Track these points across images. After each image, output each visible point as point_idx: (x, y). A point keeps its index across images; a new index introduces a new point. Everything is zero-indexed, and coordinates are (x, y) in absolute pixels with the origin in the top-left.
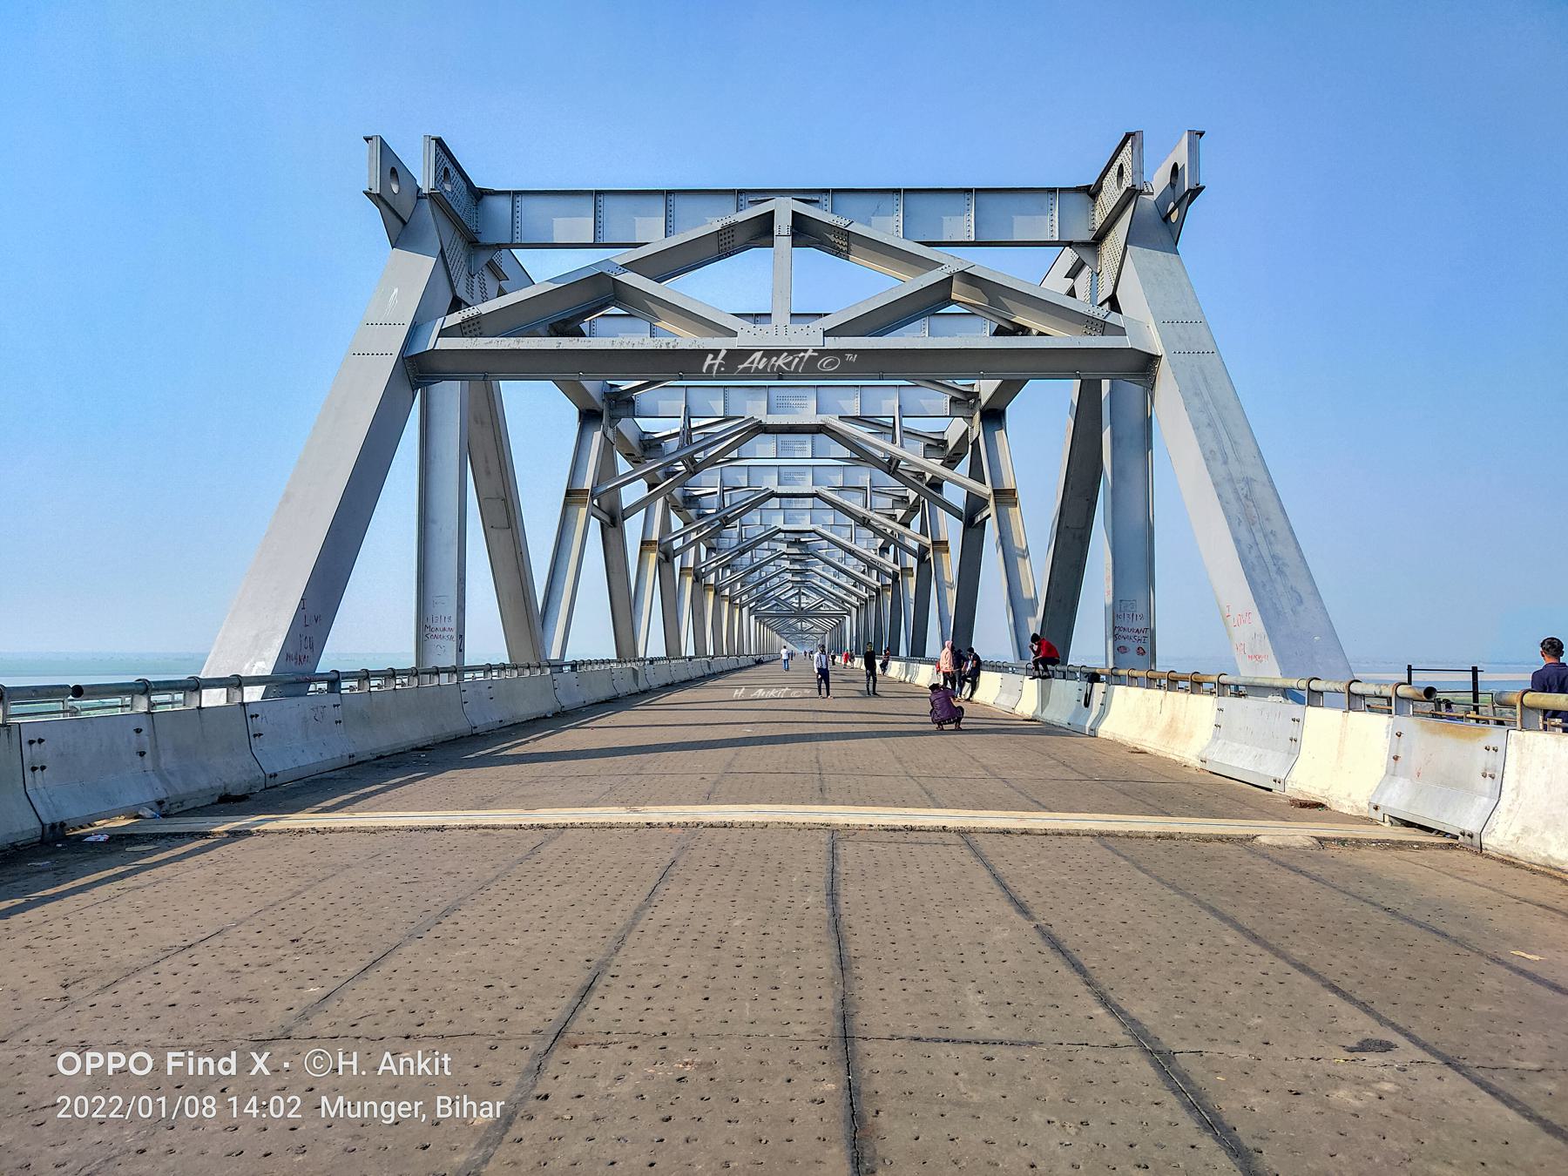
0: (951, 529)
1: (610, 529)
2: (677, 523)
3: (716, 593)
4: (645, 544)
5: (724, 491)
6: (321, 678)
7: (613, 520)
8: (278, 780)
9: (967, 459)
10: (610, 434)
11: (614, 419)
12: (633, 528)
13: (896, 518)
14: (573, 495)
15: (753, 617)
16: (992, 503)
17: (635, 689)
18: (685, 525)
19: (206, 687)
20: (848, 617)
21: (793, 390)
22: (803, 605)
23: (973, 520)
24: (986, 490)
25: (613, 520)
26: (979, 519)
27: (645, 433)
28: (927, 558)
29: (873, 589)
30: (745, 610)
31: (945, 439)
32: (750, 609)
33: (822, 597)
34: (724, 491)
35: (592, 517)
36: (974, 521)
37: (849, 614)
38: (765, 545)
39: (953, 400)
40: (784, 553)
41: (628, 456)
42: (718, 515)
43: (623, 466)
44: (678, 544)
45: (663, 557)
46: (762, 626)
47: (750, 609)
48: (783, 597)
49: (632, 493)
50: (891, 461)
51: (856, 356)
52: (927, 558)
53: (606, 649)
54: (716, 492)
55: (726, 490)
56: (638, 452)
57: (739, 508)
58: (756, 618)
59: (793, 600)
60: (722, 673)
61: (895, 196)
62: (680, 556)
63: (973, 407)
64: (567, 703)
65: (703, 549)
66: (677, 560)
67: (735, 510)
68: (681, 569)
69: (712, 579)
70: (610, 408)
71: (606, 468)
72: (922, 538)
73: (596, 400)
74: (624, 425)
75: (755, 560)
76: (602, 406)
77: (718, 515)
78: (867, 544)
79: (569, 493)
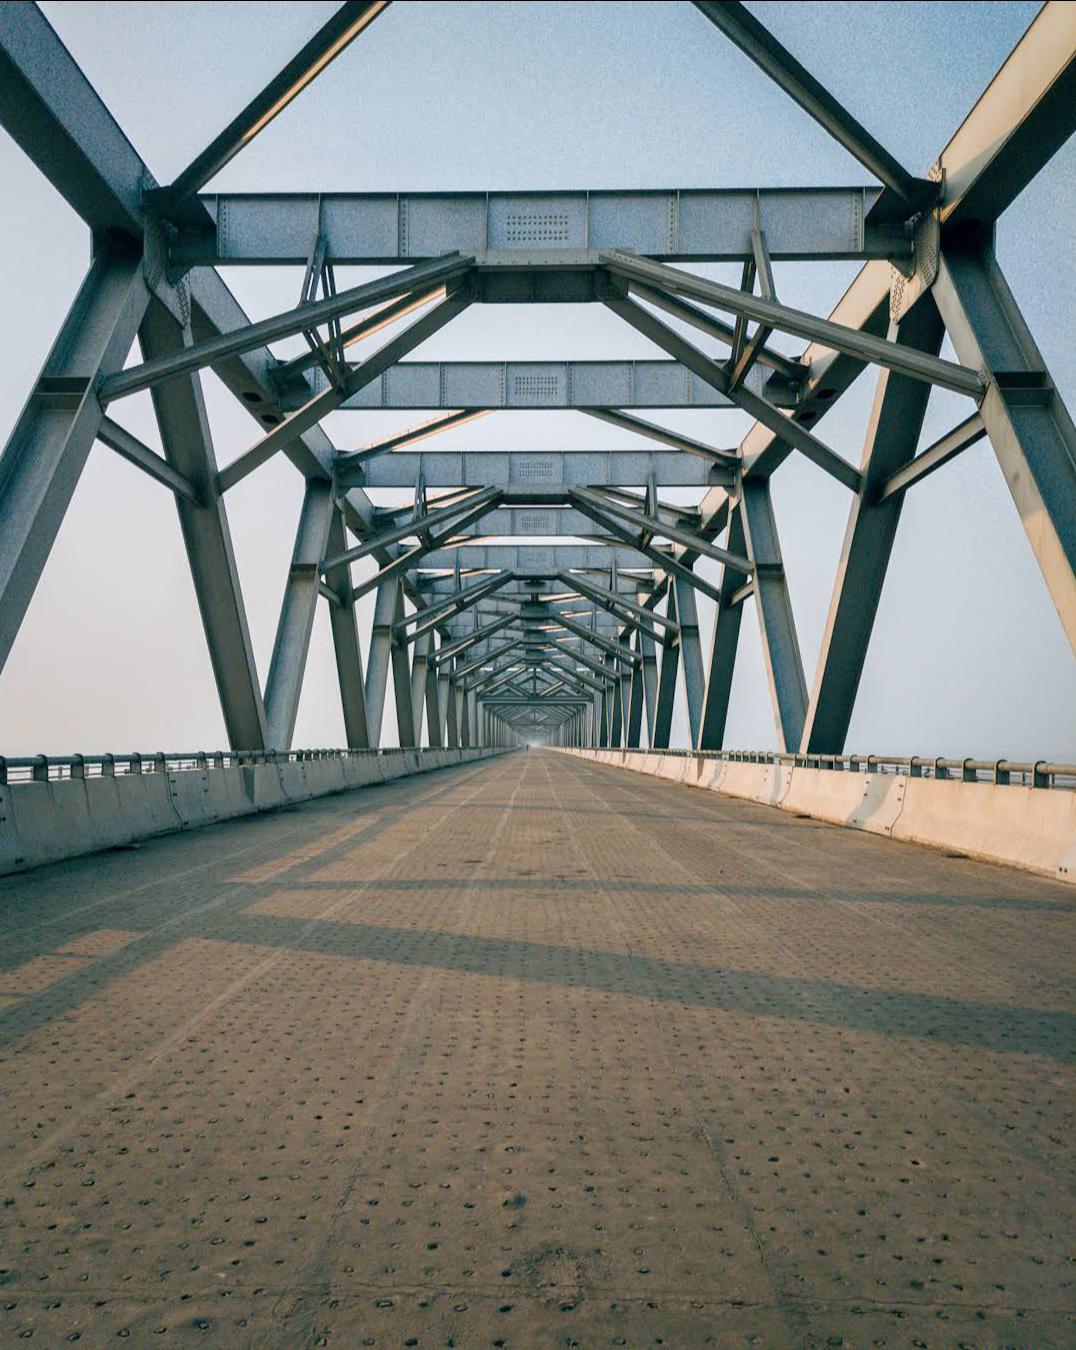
0: (706, 610)
1: (339, 611)
2: (410, 608)
3: (451, 683)
4: (378, 630)
5: (460, 574)
6: (293, 753)
7: (343, 601)
8: (188, 826)
9: (666, 599)
10: (339, 503)
11: (174, 271)
12: (365, 610)
13: (652, 586)
14: (300, 572)
15: (480, 704)
16: (680, 635)
17: (416, 769)
18: (418, 610)
19: (118, 761)
20: (590, 706)
21: (533, 511)
22: (538, 692)
23: (671, 644)
24: (676, 626)
25: (343, 601)
26: (736, 599)
27: (377, 508)
28: (674, 644)
29: (611, 679)
30: (471, 695)
31: (700, 513)
32: (478, 694)
33: (561, 680)
34: (460, 574)
35: (319, 596)
36: (882, 495)
37: (591, 699)
38: (500, 633)
39: (639, 584)
40: (521, 642)
41: (358, 532)
42: (415, 527)
43: (352, 541)
44: (411, 629)
45: (396, 643)
46: (487, 713)
47: (478, 694)
48: (515, 682)
49: (364, 570)
50: (609, 602)
51: (562, 613)
52: (674, 644)
53: (335, 737)
54: (451, 576)
55: (463, 573)
56: (267, 395)
57: (477, 591)
58: (484, 706)
59: (526, 685)
60: (449, 766)
61: (672, 200)
62: (413, 643)
63: (734, 474)
64: (189, 816)
65: (437, 637)
66: (411, 647)
67: (474, 593)
68: (415, 657)
69: (461, 683)
70: (340, 476)
71: (336, 543)
72: (670, 623)
73: (259, 381)
74: (353, 495)
75: (492, 649)
76: (332, 475)
77: (415, 527)
78: (609, 628)
79: (294, 568)
